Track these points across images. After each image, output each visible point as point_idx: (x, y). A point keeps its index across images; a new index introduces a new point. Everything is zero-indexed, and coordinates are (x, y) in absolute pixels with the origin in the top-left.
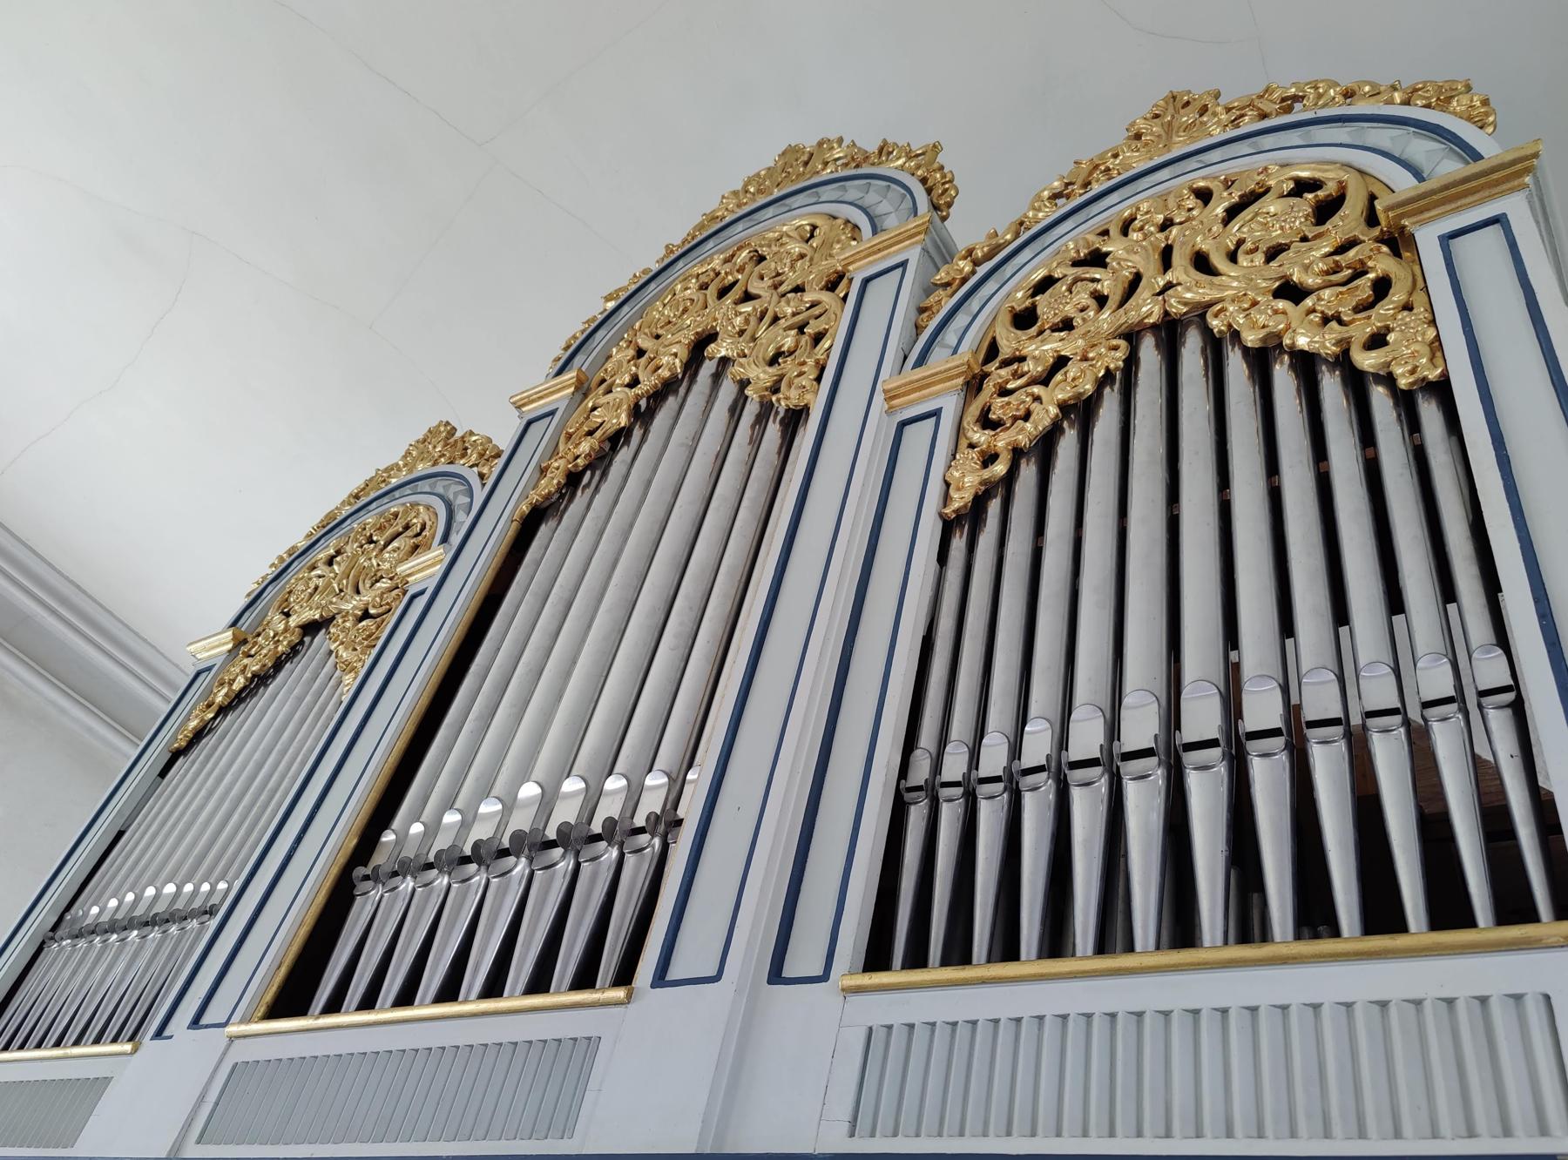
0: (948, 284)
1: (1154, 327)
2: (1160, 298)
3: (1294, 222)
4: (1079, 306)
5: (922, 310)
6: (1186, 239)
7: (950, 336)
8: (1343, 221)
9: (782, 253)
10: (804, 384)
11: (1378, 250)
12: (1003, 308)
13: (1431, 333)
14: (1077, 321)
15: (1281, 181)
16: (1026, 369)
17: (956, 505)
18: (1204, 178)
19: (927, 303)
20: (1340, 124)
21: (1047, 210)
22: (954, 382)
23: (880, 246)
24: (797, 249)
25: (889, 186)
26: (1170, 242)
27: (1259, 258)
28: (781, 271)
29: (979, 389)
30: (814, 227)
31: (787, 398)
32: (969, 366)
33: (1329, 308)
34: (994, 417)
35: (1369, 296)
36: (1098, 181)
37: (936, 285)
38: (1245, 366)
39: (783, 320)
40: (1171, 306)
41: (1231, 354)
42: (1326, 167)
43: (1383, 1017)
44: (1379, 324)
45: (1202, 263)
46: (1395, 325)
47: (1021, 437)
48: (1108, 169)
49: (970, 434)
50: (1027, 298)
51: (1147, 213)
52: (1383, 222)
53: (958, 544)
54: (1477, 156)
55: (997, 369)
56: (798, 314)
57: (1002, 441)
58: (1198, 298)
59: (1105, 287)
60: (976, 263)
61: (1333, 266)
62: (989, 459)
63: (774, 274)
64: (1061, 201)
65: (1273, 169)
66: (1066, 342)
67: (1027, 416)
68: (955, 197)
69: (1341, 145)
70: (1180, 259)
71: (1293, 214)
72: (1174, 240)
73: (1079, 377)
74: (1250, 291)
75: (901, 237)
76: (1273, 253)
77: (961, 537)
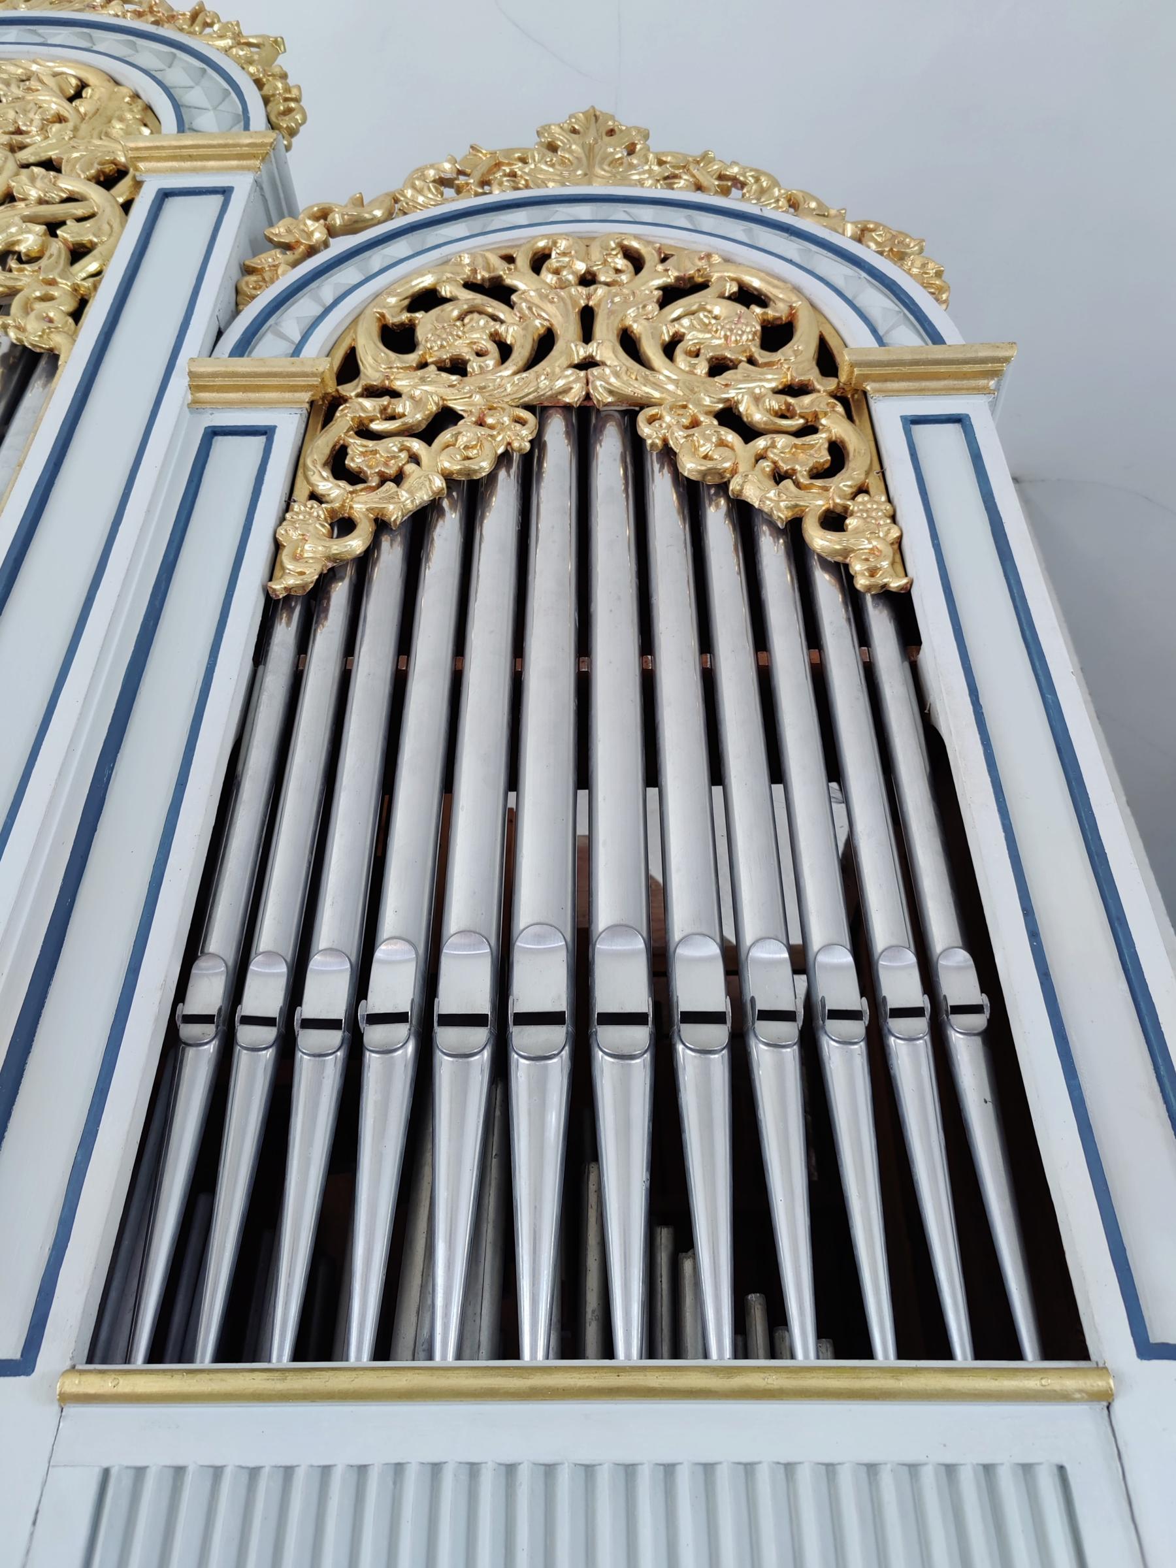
0: (287, 247)
1: (567, 408)
2: (582, 374)
3: (741, 336)
4: (475, 347)
5: (248, 270)
6: (614, 308)
7: (291, 321)
8: (796, 356)
9: (29, 102)
10: (51, 314)
11: (833, 407)
12: (368, 312)
13: (895, 533)
14: (474, 365)
15: (724, 279)
16: (400, 410)
17: (291, 581)
18: (637, 237)
19: (254, 262)
20: (786, 235)
21: (430, 196)
22: (297, 395)
23: (193, 152)
24: (54, 106)
25: (204, 71)
26: (591, 303)
27: (702, 368)
28: (24, 128)
29: (328, 418)
30: (83, 86)
31: (19, 328)
32: (323, 380)
33: (784, 460)
34: (352, 465)
35: (826, 462)
36: (501, 184)
37: (271, 241)
38: (675, 496)
39: (22, 205)
40: (595, 388)
41: (657, 475)
42: (776, 282)
43: (870, 1483)
44: (838, 501)
45: (629, 343)
46: (856, 508)
47: (391, 507)
48: (513, 175)
49: (315, 479)
50: (402, 311)
51: (564, 254)
52: (843, 376)
53: (285, 634)
54: (936, 338)
55: (358, 396)
56: (47, 203)
57: (361, 505)
58: (629, 391)
59: (510, 333)
60: (332, 232)
61: (783, 407)
62: (344, 525)
63: (12, 129)
64: (449, 192)
65: (716, 259)
66: (454, 391)
67: (399, 478)
68: (300, 125)
69: (790, 261)
70: (604, 330)
71: (739, 326)
72: (599, 305)
73: (473, 447)
74: (693, 405)
75: (226, 151)
76: (718, 367)
77: (288, 624)
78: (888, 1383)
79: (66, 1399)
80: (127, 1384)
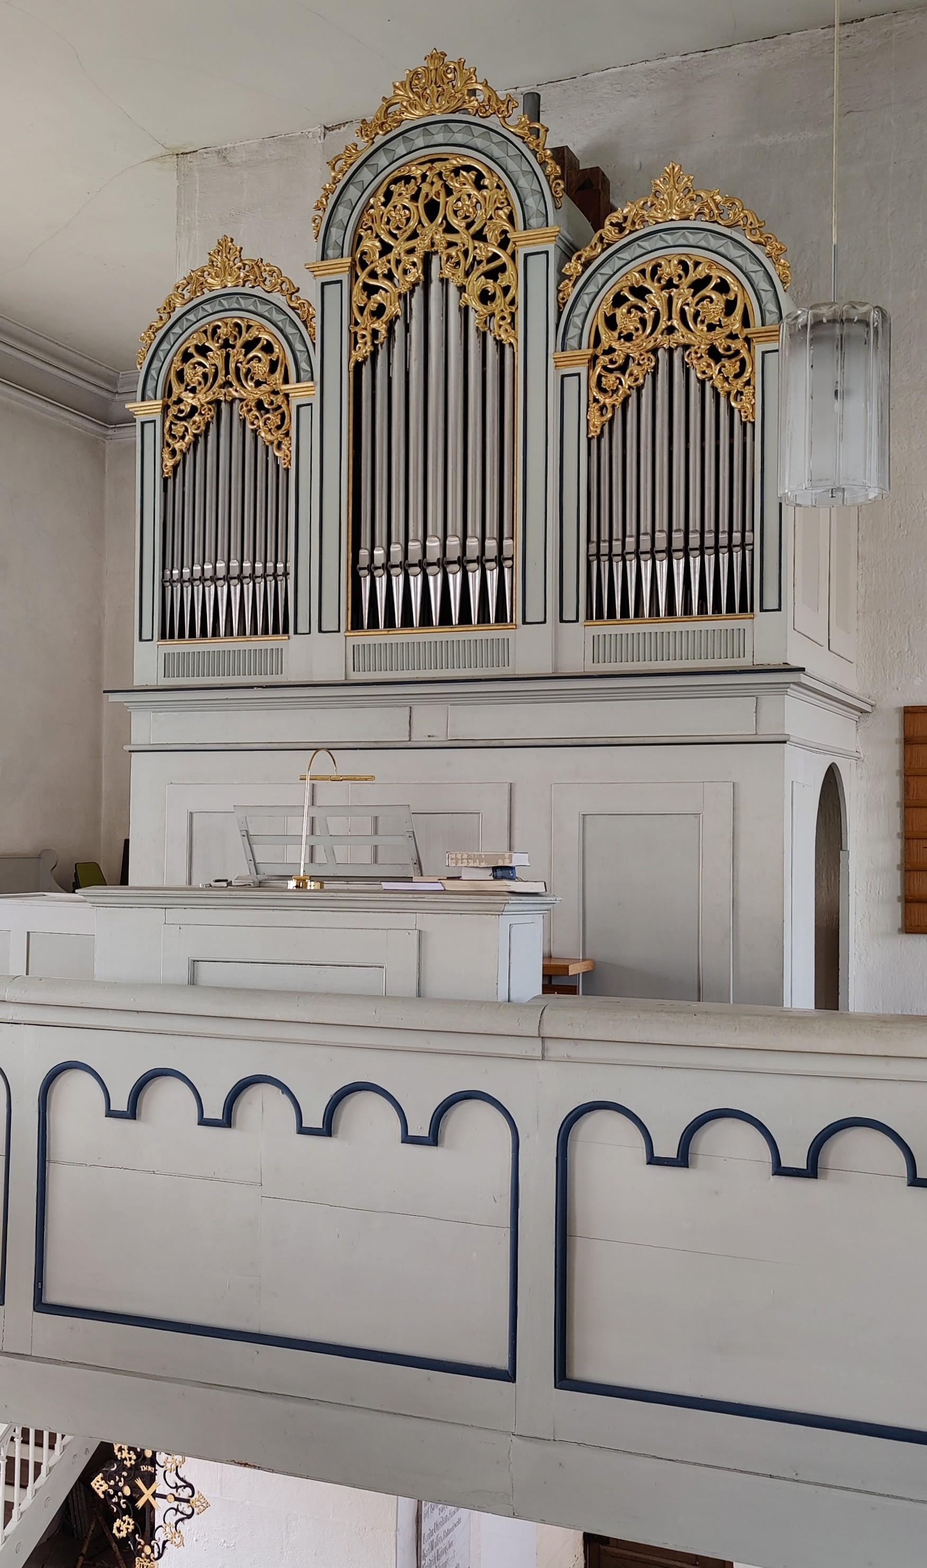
78: (249, 639)
79: (585, 626)
80: (279, 638)
